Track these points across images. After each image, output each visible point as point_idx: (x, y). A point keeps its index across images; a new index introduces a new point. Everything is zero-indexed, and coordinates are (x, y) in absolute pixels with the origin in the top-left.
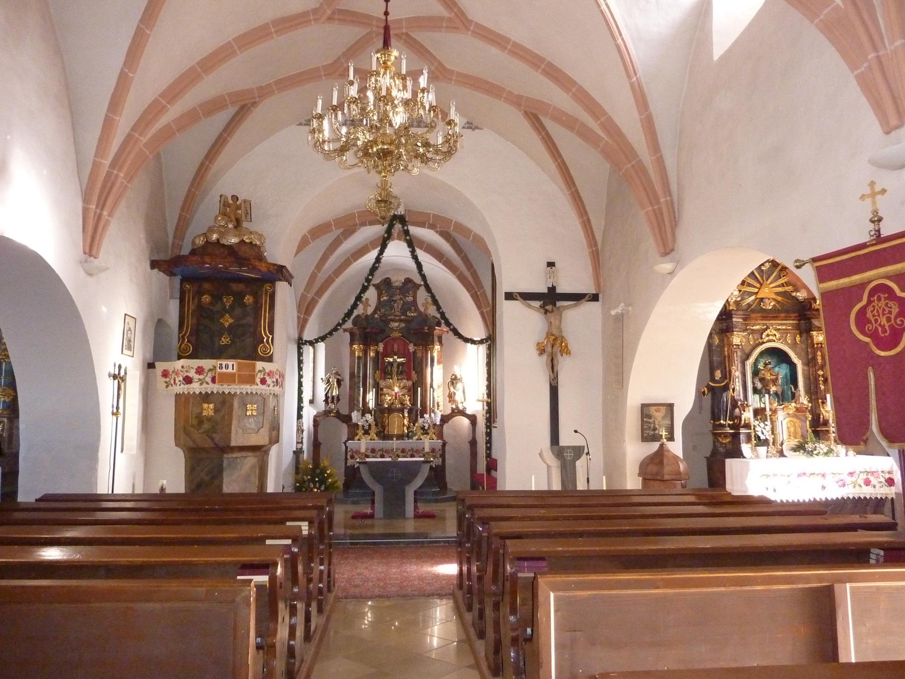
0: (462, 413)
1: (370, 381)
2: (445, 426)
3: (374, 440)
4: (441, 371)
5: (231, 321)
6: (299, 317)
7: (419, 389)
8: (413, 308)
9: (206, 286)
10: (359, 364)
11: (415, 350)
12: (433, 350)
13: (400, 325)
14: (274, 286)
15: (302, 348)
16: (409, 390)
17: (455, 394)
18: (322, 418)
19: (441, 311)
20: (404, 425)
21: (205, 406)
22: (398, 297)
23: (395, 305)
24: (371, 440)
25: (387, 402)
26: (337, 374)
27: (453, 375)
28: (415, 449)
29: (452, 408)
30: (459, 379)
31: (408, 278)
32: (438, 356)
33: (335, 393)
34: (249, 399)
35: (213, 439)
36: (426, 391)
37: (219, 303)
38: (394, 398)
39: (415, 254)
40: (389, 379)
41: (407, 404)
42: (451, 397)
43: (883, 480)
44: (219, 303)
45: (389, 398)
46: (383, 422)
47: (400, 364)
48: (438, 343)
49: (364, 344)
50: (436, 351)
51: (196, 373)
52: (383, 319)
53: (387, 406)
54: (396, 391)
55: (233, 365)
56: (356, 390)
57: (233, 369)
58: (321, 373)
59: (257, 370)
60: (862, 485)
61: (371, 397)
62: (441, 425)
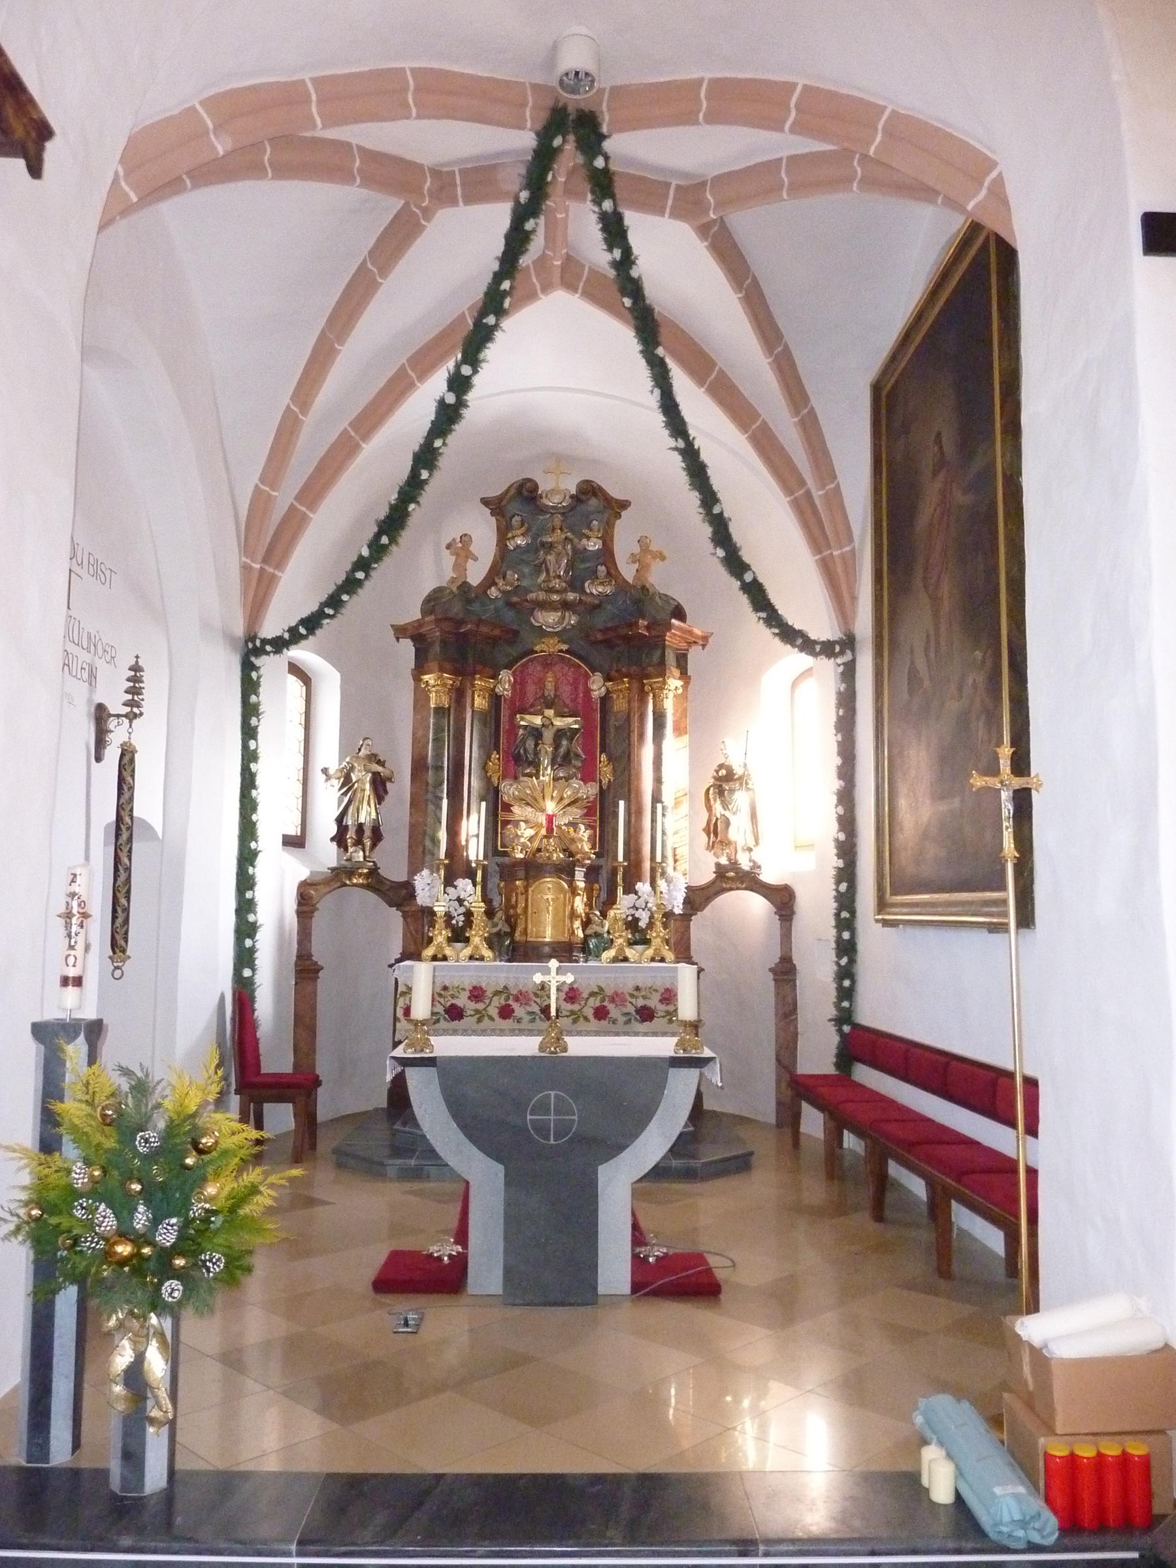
0: (750, 881)
1: (472, 782)
2: (696, 921)
3: (482, 959)
4: (685, 754)
6: (246, 568)
7: (622, 803)
8: (602, 569)
10: (438, 730)
11: (608, 692)
12: (662, 689)
13: (563, 618)
15: (255, 668)
16: (589, 812)
17: (727, 823)
19: (716, 510)
20: (573, 915)
22: (558, 536)
23: (551, 558)
24: (471, 958)
25: (524, 846)
26: (373, 758)
27: (721, 766)
28: (609, 992)
29: (718, 865)
30: (740, 778)
31: (587, 482)
32: (676, 711)
33: (366, 814)
36: (639, 812)
38: (543, 832)
39: (634, 273)
40: (530, 775)
41: (581, 851)
42: (715, 832)
43: (632, 1010)
45: (530, 832)
46: (509, 906)
47: (560, 734)
48: (677, 673)
49: (455, 672)
50: (671, 695)
51: (469, 998)
52: (515, 599)
53: (521, 856)
54: (550, 813)
56: (431, 807)
58: (328, 753)
60: (496, 1016)
61: (473, 830)
62: (686, 917)
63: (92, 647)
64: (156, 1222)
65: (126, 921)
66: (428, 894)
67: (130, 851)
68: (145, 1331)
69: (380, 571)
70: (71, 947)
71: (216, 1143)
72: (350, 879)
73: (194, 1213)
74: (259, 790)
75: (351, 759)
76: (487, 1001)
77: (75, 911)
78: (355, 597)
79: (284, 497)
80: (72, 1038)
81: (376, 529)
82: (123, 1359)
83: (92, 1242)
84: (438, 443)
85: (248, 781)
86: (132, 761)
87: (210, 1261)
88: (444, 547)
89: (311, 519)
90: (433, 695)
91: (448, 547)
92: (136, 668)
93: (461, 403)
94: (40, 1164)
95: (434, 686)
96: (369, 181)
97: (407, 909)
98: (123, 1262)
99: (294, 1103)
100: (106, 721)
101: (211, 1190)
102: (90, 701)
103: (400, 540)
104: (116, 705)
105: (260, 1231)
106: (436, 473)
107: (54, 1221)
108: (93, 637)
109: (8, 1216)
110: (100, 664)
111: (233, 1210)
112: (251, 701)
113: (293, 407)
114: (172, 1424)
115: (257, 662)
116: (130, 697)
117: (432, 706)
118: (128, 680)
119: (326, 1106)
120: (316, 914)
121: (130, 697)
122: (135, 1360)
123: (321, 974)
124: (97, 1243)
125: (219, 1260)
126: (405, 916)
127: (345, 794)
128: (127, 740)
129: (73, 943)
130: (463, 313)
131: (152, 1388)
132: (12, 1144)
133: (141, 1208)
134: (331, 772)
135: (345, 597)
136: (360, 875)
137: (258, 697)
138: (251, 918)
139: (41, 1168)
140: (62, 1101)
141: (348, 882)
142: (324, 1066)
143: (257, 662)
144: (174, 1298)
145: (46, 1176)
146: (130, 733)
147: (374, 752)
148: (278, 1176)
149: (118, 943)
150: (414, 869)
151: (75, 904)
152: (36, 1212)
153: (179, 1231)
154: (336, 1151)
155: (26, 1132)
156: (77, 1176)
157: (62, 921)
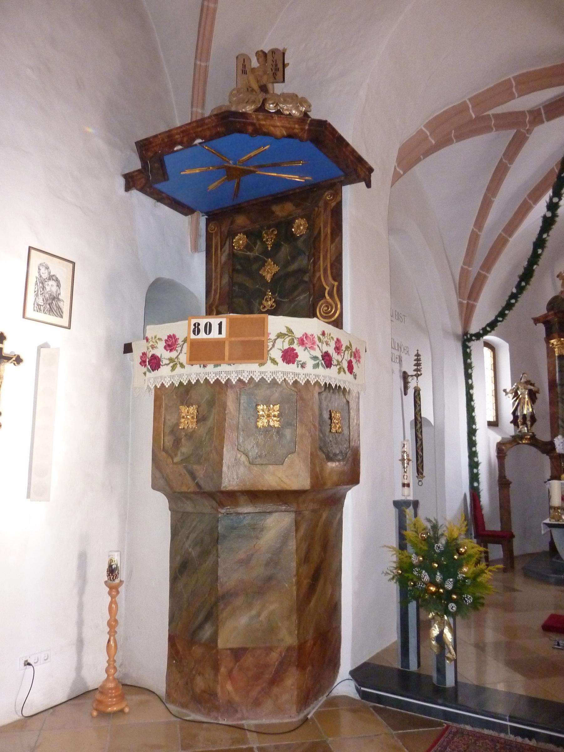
5: (276, 269)
6: (460, 304)
9: (241, 220)
14: (338, 194)
15: (469, 347)
18: (508, 446)
21: (184, 410)
26: (528, 382)
33: (527, 410)
34: (262, 393)
35: (193, 476)
37: (259, 243)
44: (259, 243)
51: (165, 348)
55: (220, 325)
57: (220, 333)
58: (506, 382)
59: (273, 337)
60: (279, 360)
63: (400, 349)
64: (444, 580)
65: (422, 461)
66: (562, 447)
67: (421, 432)
68: (443, 621)
69: (523, 298)
70: (405, 472)
71: (466, 551)
72: (521, 441)
73: (459, 578)
74: (475, 402)
75: (517, 384)
76: (179, 349)
77: (405, 458)
78: (511, 311)
79: (475, 269)
80: (408, 506)
81: (518, 280)
82: (435, 632)
83: (421, 585)
84: (545, 236)
85: (470, 398)
86: (419, 394)
87: (467, 598)
88: (556, 275)
89: (488, 277)
90: (556, 350)
91: (558, 276)
92: (418, 355)
93: (554, 215)
94: (400, 554)
95: (556, 345)
96: (499, 127)
97: (552, 455)
98: (433, 593)
99: (502, 544)
100: (407, 379)
101: (465, 570)
102: (400, 370)
103: (531, 283)
104: (411, 372)
105: (486, 588)
106: (546, 250)
107: (406, 575)
108: (399, 345)
109: (389, 572)
110: (404, 356)
111: (475, 579)
112: (468, 362)
113: (475, 230)
114: (455, 661)
115: (469, 344)
116: (416, 367)
117: (557, 355)
118: (415, 360)
119: (518, 547)
120: (506, 457)
121: (416, 367)
122: (440, 633)
123: (511, 485)
124: (423, 585)
125: (470, 598)
126: (551, 458)
127: (516, 400)
128: (416, 385)
129: (405, 471)
130: (553, 167)
131: (447, 645)
132: (389, 545)
133: (438, 574)
134: (508, 391)
135: (507, 312)
136: (526, 439)
137: (471, 360)
138: (476, 459)
139: (400, 555)
140: (406, 530)
141: (520, 442)
142: (516, 530)
143: (469, 344)
144: (453, 610)
145: (402, 558)
146: (417, 383)
147: (528, 379)
148: (493, 567)
149: (420, 471)
150: (554, 435)
151: (405, 455)
152: (400, 572)
153: (453, 584)
154: (523, 569)
155: (393, 541)
156: (414, 559)
157: (400, 462)
